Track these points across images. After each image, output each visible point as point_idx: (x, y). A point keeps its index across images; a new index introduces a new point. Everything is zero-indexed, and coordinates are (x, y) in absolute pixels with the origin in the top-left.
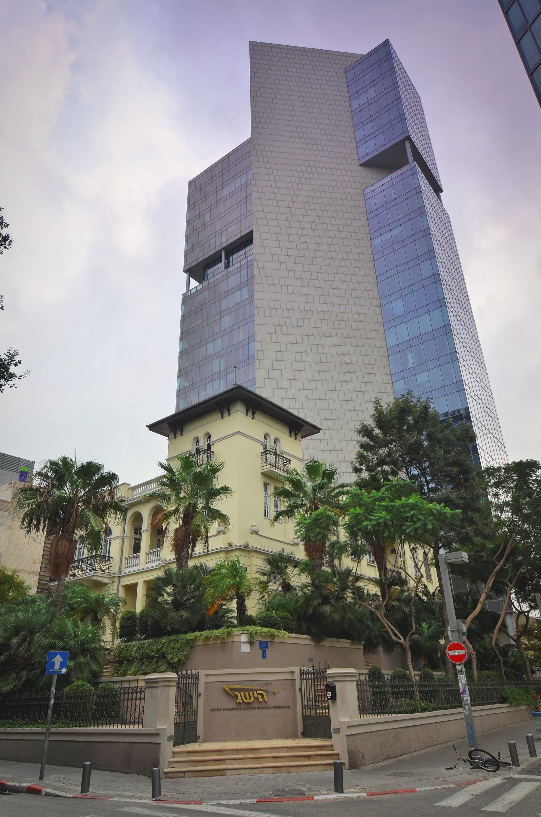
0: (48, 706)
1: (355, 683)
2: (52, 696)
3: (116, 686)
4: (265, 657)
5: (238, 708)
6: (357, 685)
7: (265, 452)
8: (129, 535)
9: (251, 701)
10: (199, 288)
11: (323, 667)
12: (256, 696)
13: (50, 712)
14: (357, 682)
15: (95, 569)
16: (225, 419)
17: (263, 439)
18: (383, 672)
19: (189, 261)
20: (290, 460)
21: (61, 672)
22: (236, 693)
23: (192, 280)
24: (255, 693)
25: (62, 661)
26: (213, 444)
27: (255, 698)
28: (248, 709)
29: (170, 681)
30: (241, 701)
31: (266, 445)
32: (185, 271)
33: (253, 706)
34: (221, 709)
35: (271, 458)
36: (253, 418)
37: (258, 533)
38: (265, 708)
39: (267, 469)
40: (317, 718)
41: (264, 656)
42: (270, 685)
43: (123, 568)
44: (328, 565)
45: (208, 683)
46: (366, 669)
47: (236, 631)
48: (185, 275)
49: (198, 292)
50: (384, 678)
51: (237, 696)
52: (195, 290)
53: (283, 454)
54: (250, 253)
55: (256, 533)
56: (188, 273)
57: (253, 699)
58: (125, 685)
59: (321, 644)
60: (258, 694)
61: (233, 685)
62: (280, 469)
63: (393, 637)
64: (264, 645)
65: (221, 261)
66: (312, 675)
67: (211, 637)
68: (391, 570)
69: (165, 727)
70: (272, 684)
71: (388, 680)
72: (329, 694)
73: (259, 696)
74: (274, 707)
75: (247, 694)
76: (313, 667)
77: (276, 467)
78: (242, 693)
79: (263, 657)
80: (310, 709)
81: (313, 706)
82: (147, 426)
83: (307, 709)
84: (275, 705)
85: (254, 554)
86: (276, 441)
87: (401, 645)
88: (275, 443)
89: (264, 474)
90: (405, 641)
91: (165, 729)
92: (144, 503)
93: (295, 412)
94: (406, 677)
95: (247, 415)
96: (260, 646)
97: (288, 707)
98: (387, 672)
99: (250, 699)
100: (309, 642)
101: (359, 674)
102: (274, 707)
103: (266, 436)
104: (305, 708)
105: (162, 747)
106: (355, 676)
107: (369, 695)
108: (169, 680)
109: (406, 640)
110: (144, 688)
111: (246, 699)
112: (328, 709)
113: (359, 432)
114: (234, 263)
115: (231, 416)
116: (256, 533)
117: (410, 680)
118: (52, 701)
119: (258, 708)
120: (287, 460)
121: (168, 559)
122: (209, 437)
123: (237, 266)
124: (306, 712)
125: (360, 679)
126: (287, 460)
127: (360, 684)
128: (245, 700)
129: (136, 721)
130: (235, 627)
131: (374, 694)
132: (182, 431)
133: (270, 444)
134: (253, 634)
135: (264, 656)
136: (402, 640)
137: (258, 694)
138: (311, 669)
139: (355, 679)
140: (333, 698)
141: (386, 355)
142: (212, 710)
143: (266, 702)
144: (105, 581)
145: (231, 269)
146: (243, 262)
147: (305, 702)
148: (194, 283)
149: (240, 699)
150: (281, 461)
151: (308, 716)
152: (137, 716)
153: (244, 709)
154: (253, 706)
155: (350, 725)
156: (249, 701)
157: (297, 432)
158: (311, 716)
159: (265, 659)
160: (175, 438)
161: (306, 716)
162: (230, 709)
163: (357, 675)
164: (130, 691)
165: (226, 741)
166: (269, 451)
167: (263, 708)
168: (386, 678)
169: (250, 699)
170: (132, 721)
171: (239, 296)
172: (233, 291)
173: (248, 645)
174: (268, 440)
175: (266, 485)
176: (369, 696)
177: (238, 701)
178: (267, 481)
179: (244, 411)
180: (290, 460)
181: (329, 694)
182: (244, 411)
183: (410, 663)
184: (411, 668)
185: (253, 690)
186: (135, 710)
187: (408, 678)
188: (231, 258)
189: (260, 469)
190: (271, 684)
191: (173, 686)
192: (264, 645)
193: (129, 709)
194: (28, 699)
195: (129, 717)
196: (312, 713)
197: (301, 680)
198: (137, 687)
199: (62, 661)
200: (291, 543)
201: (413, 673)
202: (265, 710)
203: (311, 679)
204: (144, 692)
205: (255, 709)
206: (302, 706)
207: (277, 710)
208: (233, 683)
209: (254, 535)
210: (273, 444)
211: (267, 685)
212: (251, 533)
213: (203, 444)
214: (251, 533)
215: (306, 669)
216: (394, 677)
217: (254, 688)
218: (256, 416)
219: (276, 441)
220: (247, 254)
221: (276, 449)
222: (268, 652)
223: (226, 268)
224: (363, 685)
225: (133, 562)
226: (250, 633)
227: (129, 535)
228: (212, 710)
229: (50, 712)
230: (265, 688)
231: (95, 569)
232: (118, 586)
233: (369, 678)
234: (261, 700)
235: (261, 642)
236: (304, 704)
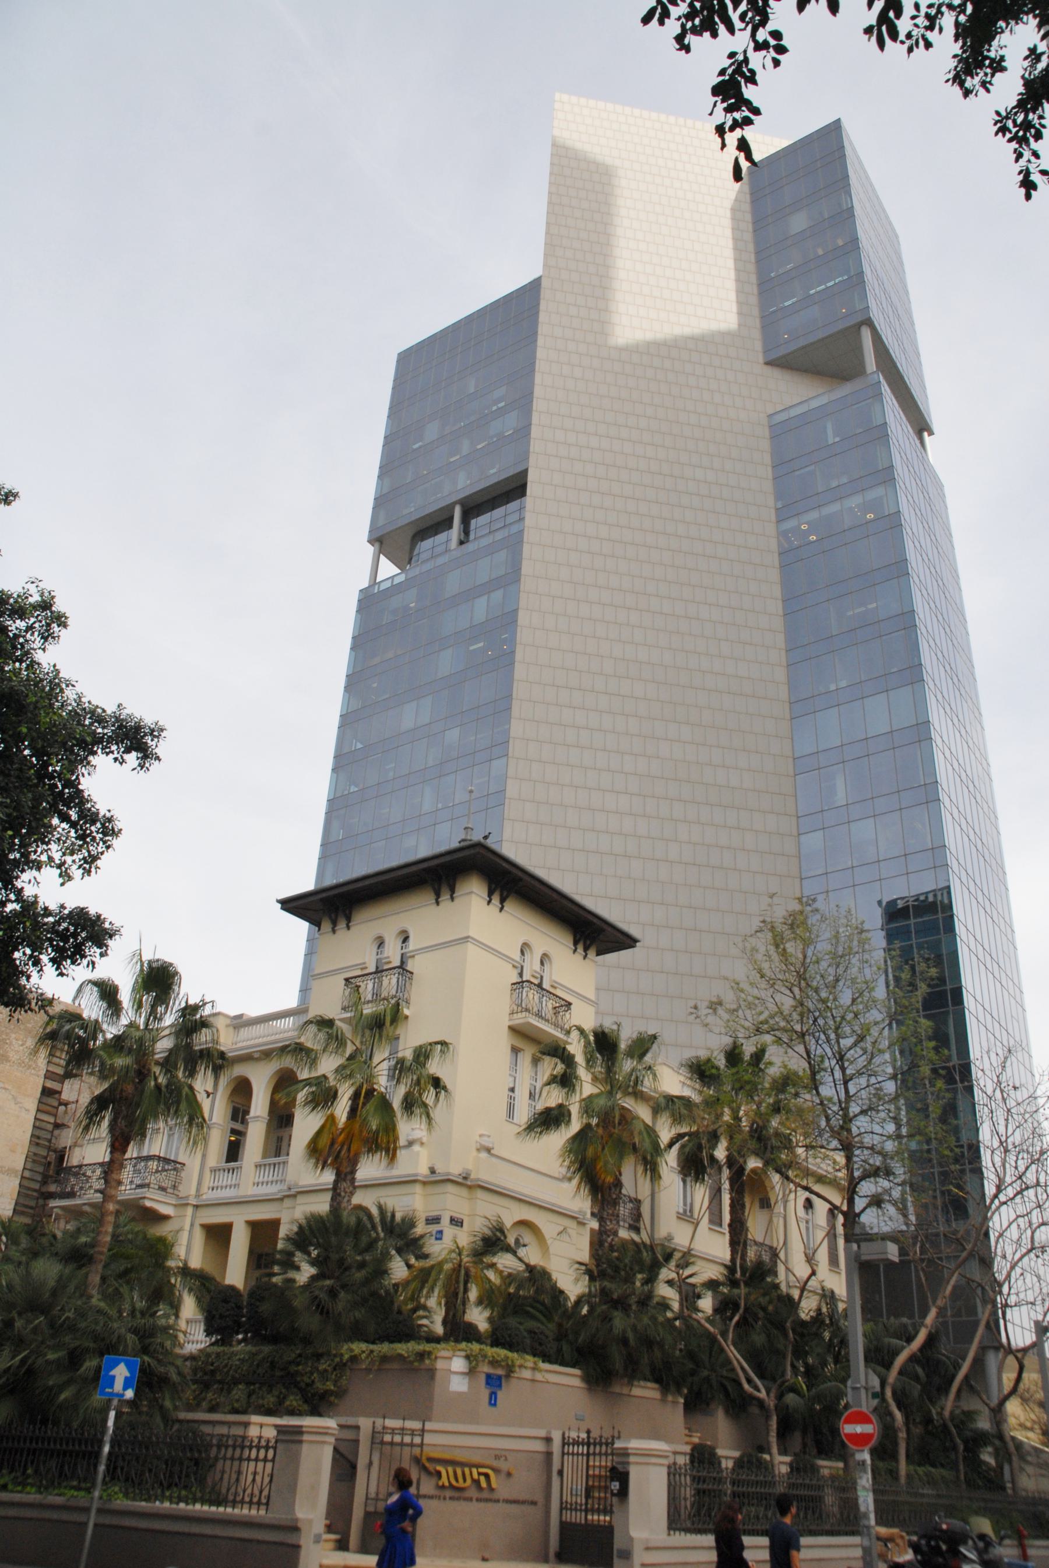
0: (97, 1454)
1: (664, 1471)
2: (107, 1438)
3: (207, 1429)
4: (495, 1405)
6: (669, 1474)
7: (520, 984)
8: (221, 1122)
10: (397, 581)
11: (607, 1434)
12: (476, 1476)
13: (102, 1468)
14: (669, 1467)
15: (148, 1186)
16: (442, 905)
17: (516, 956)
18: (720, 1452)
19: (381, 522)
20: (570, 1004)
21: (123, 1395)
22: (439, 1468)
24: (474, 1471)
25: (128, 1375)
26: (413, 956)
27: (473, 1480)
28: (459, 1499)
29: (326, 1434)
30: (447, 1484)
31: (522, 967)
33: (467, 1494)
35: (531, 996)
39: (520, 1019)
40: (589, 1528)
41: (493, 1401)
43: (204, 1189)
44: (627, 1225)
46: (687, 1443)
47: (443, 1351)
48: (370, 550)
49: (396, 589)
50: (720, 1463)
52: (388, 584)
53: (555, 988)
54: (516, 517)
55: (488, 1150)
56: (377, 545)
57: (469, 1481)
58: (223, 1430)
59: (611, 1390)
60: (479, 1474)
62: (547, 1021)
63: (746, 1386)
64: (494, 1383)
65: (450, 527)
66: (585, 1448)
68: (756, 1243)
69: (311, 1516)
71: (727, 1469)
72: (615, 1486)
73: (482, 1478)
74: (507, 1501)
75: (459, 1471)
76: (588, 1432)
77: (539, 1015)
78: (450, 1469)
79: (490, 1403)
80: (576, 1510)
81: (581, 1505)
82: (278, 901)
83: (571, 1509)
84: (510, 1498)
85: (480, 1194)
86: (544, 959)
87: (761, 1403)
88: (542, 963)
89: (514, 1030)
90: (768, 1394)
91: (310, 1521)
92: (258, 1059)
93: (589, 903)
94: (767, 1468)
96: (487, 1383)
97: (534, 1503)
98: (728, 1455)
99: (465, 1480)
100: (577, 1382)
101: (675, 1453)
102: (507, 1501)
103: (525, 948)
104: (566, 1509)
105: (303, 1553)
106: (666, 1457)
107: (688, 1492)
108: (324, 1432)
109: (772, 1395)
110: (273, 1441)
111: (457, 1480)
112: (611, 1512)
114: (479, 534)
115: (456, 901)
116: (488, 1150)
117: (1002, 1539)
118: (106, 1449)
119: (478, 1500)
120: (563, 1003)
121: (301, 1183)
122: (406, 939)
123: (484, 542)
124: (569, 1517)
125: (675, 1464)
126: (563, 1003)
127: (673, 1471)
128: (454, 1483)
129: (255, 1500)
130: (437, 1340)
131: (699, 1492)
132: (349, 919)
133: (532, 966)
135: (493, 1401)
136: (763, 1394)
137: (479, 1474)
138: (584, 1435)
139: (665, 1462)
140: (623, 1493)
141: (791, 773)
144: (164, 1210)
145: (470, 547)
146: (499, 536)
147: (567, 1497)
148: (388, 569)
149: (444, 1480)
150: (551, 1004)
151: (571, 1523)
152: (256, 1492)
153: (451, 1498)
154: (467, 1494)
155: (650, 1545)
156: (461, 1484)
157: (588, 942)
158: (575, 1524)
159: (493, 1409)
160: (334, 931)
161: (566, 1523)
163: (670, 1454)
164: (230, 1442)
166: (528, 981)
168: (723, 1465)
169: (465, 1480)
170: (247, 1499)
171: (480, 609)
172: (469, 595)
174: (527, 956)
175: (515, 1050)
176: (688, 1496)
177: (440, 1483)
178: (519, 1044)
180: (570, 1004)
181: (615, 1486)
182: (485, 895)
183: (773, 1439)
184: (775, 1450)
185: (471, 1466)
186: (254, 1480)
187: (766, 1469)
188: (473, 522)
189: (507, 1018)
191: (330, 1443)
192: (494, 1383)
193: (226, 1476)
194: (61, 1439)
195: (224, 1491)
196: (578, 1518)
197: (563, 1454)
198: (244, 1438)
199: (128, 1375)
200: (556, 1175)
201: (779, 1458)
202: (490, 1505)
203: (582, 1454)
204: (275, 1448)
205: (471, 1499)
206: (562, 1503)
207: (513, 1506)
209: (484, 1155)
210: (537, 966)
211: (497, 1457)
212: (478, 1150)
213: (393, 953)
214: (478, 1150)
215: (574, 1435)
216: (739, 1463)
218: (508, 906)
219: (544, 959)
220: (509, 520)
221: (542, 977)
222: (500, 1394)
223: (461, 543)
224: (680, 1475)
225: (226, 1179)
227: (221, 1122)
229: (102, 1468)
230: (495, 1464)
231: (148, 1186)
232: (192, 1225)
233: (692, 1462)
234: (484, 1484)
235: (489, 1377)
236: (564, 1499)
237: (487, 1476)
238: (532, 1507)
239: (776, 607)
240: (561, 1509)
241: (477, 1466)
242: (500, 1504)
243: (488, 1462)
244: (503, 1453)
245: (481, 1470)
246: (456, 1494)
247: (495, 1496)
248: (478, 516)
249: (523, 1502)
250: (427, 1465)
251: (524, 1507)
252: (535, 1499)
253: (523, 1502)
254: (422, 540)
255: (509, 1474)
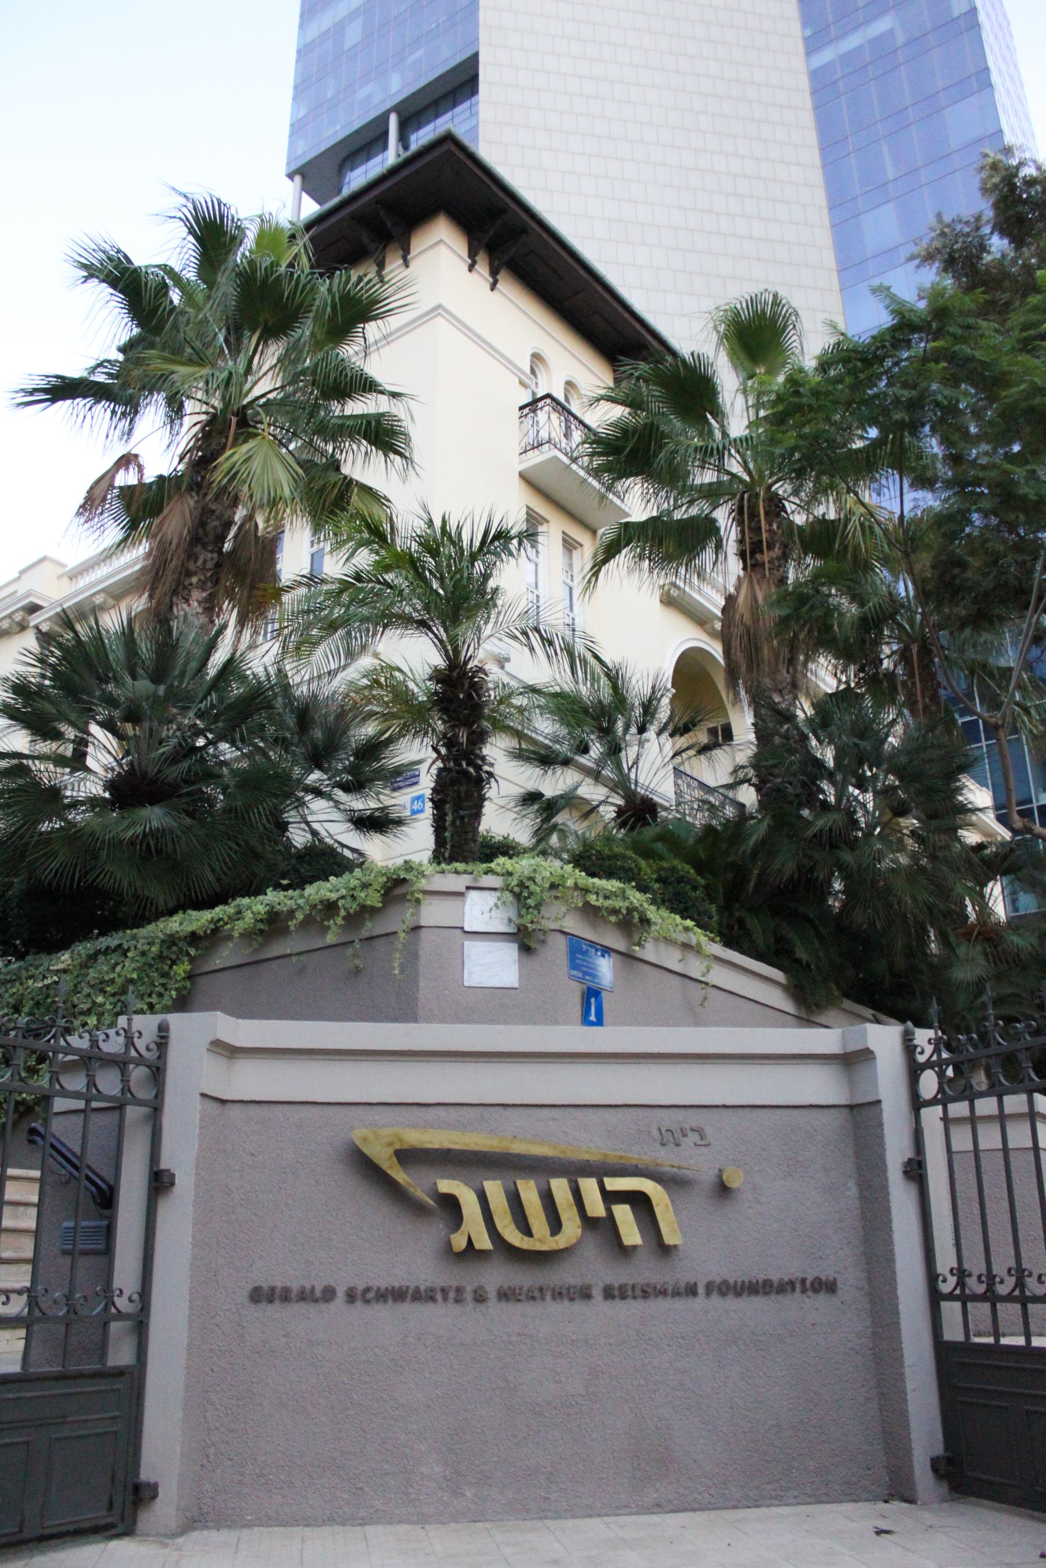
5: (459, 1290)
9: (561, 1241)
12: (596, 1207)
22: (446, 1186)
23: (306, 198)
27: (589, 1222)
30: (484, 1242)
32: (291, 176)
34: (329, 1294)
36: (493, 287)
37: (507, 665)
38: (664, 1293)
42: (694, 1137)
45: (234, 1111)
51: (451, 1204)
57: (572, 1228)
60: (610, 1198)
61: (427, 1126)
65: (385, 148)
67: (291, 913)
70: (709, 1131)
73: (623, 1213)
74: (724, 1289)
78: (494, 1189)
80: (991, 1297)
95: (471, 268)
97: (827, 1287)
99: (555, 1225)
102: (724, 1289)
113: (929, 257)
119: (609, 1293)
134: (533, 887)
137: (610, 1198)
142: (259, 1296)
143: (664, 1250)
151: (967, 1347)
153: (505, 1295)
156: (542, 1239)
161: (953, 1346)
162: (398, 1295)
165: (364, 1522)
167: (647, 1292)
169: (555, 1225)
173: (509, 952)
177: (459, 1242)
178: (542, 508)
179: (462, 248)
182: (464, 252)
185: (574, 1171)
190: (699, 1131)
205: (585, 1294)
208: (431, 1113)
211: (671, 1138)
217: (583, 1155)
226: (521, 884)
228: (259, 1296)
230: (666, 1158)
234: (631, 1233)
236: (945, 1260)
237: (639, 1202)
238: (822, 1299)
239: (813, 157)
240: (935, 1298)
241: (600, 1171)
242: (699, 1302)
243: (636, 1155)
244: (694, 1119)
245: (614, 1184)
246: (523, 1278)
247: (681, 1273)
248: (419, 128)
249: (785, 1287)
250: (400, 1175)
251: (793, 1304)
252: (826, 1273)
253: (785, 1287)
254: (352, 169)
255: (723, 1190)
